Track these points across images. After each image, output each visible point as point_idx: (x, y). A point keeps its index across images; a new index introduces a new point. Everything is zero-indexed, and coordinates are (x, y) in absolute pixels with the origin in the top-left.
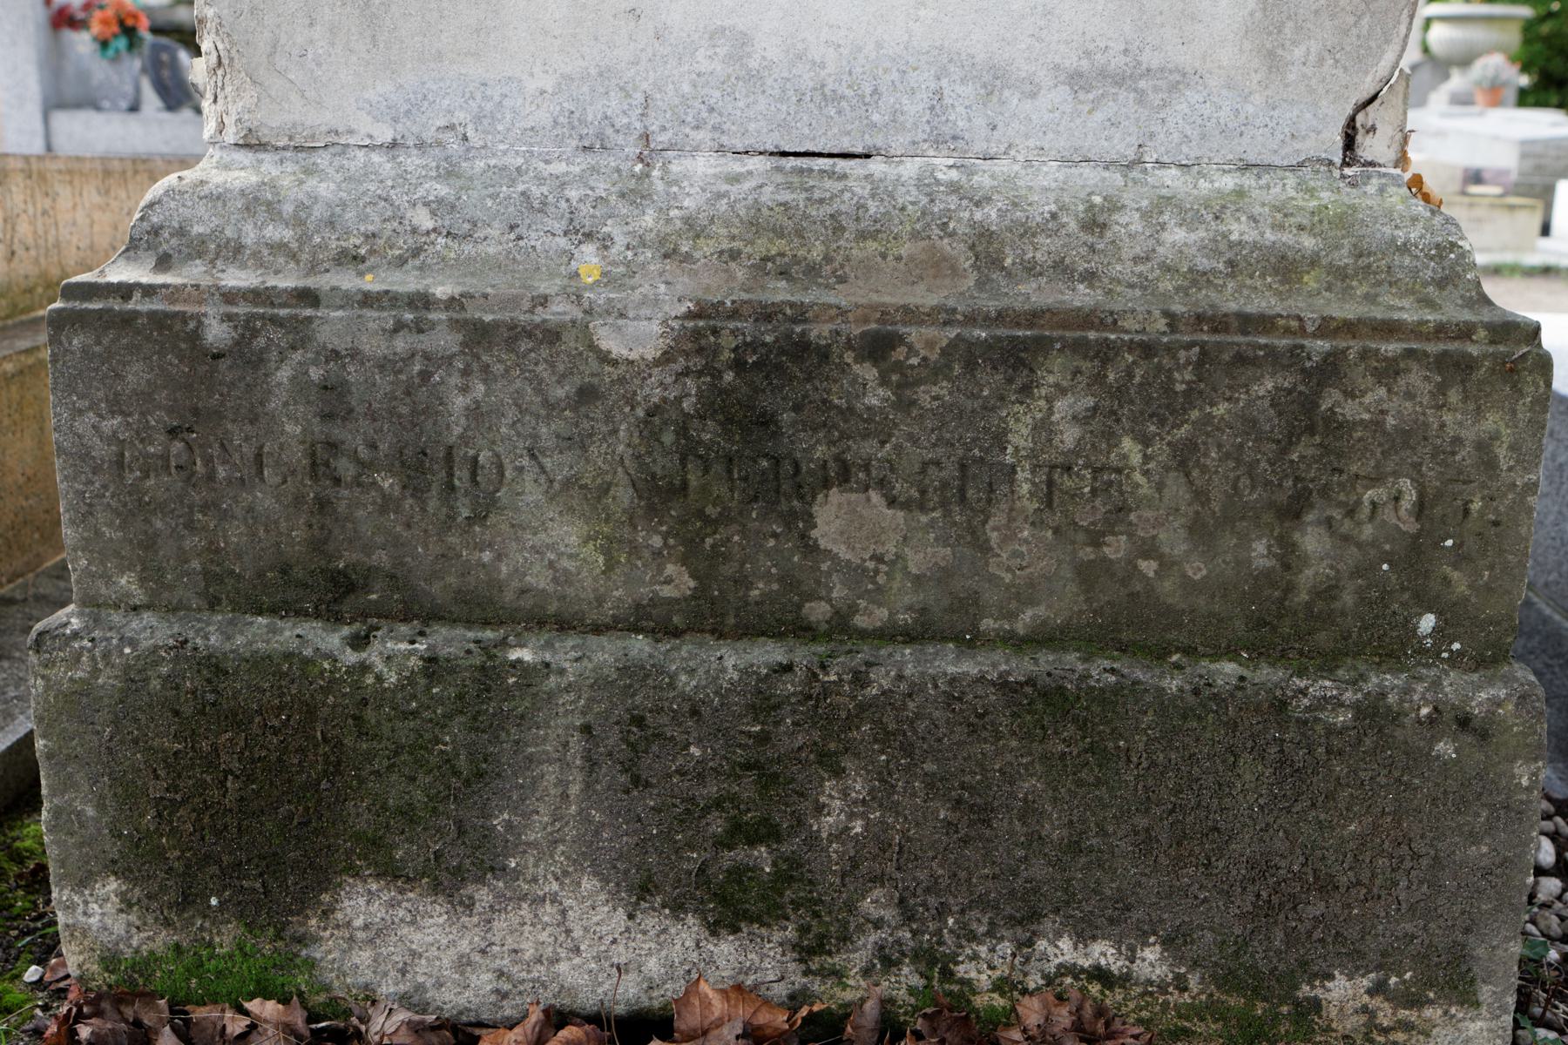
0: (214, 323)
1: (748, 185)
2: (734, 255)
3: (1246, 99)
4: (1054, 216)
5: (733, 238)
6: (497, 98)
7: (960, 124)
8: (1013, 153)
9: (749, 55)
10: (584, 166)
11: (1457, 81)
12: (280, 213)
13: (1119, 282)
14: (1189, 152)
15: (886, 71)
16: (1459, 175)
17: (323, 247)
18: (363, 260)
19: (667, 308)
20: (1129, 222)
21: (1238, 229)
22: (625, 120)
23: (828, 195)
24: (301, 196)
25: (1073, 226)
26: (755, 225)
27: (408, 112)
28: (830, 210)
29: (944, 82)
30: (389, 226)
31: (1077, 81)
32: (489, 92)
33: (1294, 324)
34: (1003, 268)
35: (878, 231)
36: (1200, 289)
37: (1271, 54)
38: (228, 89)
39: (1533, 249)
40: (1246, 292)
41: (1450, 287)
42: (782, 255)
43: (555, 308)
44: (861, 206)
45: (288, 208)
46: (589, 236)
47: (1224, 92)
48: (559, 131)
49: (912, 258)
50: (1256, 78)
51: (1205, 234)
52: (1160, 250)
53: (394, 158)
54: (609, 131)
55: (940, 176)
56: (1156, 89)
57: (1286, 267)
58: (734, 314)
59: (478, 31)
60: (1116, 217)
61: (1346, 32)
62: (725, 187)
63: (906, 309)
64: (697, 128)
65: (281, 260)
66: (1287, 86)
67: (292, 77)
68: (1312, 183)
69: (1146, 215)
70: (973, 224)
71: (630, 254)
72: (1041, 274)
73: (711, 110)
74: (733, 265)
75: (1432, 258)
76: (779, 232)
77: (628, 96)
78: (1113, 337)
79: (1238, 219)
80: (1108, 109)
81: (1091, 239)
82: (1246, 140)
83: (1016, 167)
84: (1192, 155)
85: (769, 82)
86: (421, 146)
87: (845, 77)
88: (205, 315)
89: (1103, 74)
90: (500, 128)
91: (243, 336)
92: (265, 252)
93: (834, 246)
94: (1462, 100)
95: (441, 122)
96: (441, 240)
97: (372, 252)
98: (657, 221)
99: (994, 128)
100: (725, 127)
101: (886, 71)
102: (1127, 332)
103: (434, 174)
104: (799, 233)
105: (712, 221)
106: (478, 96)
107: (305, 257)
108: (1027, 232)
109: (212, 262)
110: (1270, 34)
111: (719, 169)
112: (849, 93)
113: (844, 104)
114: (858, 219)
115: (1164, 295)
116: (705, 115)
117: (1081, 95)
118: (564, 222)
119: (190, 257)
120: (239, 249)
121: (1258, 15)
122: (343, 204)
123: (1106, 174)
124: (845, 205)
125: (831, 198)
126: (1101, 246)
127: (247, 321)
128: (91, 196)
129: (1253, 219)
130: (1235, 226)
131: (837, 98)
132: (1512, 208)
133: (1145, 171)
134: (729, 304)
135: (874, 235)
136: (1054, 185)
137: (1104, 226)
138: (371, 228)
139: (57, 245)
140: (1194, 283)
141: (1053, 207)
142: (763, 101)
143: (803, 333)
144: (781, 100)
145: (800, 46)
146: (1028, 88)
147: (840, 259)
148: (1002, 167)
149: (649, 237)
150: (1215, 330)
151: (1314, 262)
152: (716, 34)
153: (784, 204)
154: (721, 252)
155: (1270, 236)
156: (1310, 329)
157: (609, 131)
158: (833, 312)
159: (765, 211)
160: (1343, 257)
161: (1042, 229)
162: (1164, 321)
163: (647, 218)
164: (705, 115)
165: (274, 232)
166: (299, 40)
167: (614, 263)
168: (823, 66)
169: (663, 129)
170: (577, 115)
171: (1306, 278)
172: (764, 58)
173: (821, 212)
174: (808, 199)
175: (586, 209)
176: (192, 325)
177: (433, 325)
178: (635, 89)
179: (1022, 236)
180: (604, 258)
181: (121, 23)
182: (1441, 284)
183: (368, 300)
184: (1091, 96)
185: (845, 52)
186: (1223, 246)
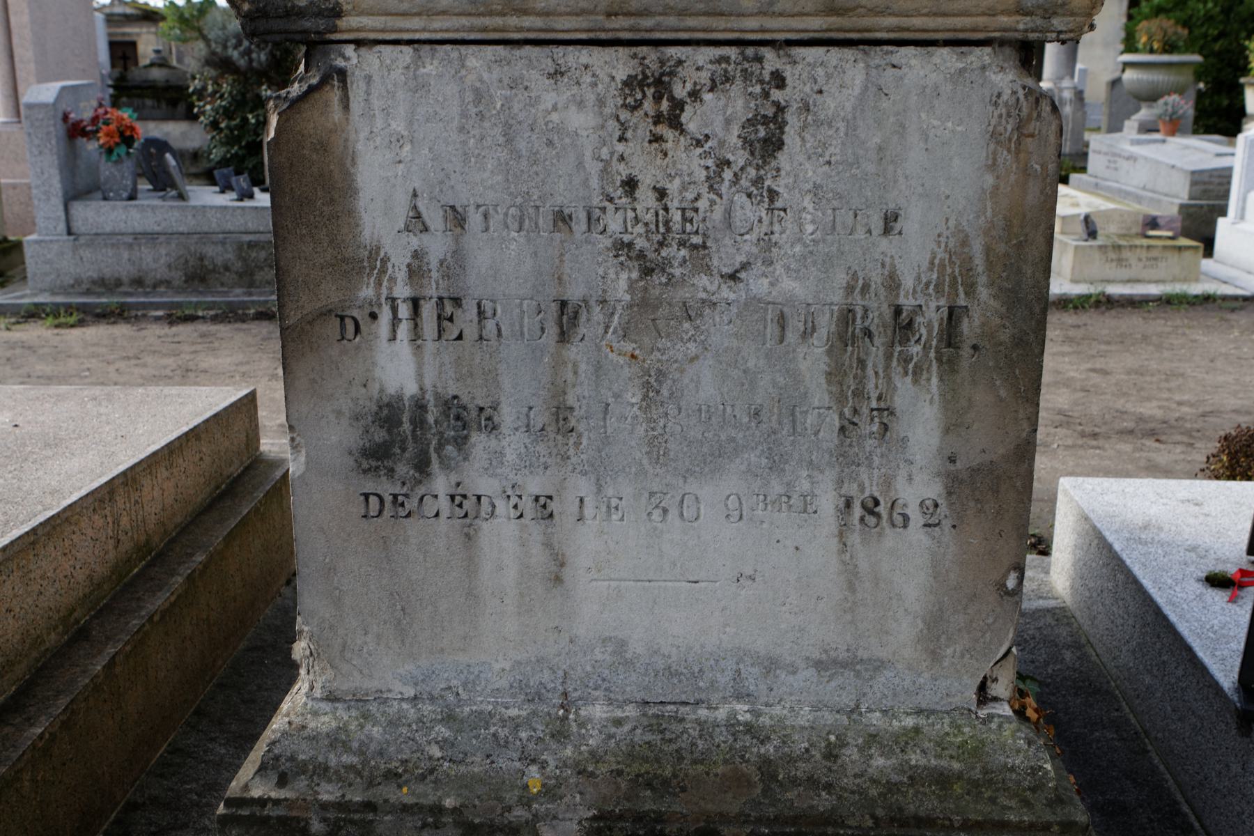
0: (316, 823)
1: (627, 728)
2: (620, 773)
3: (919, 675)
4: (807, 750)
5: (619, 763)
6: (476, 673)
7: (751, 688)
8: (783, 703)
9: (626, 651)
10: (529, 711)
11: (1144, 113)
12: (350, 748)
13: (846, 790)
14: (887, 703)
15: (707, 660)
16: (1141, 218)
17: (377, 767)
18: (400, 776)
19: (581, 813)
20: (851, 754)
21: (915, 758)
22: (553, 685)
23: (674, 736)
24: (363, 737)
25: (818, 756)
26: (631, 756)
27: (423, 681)
28: (674, 747)
29: (741, 666)
30: (415, 755)
31: (819, 665)
32: (472, 670)
33: (947, 823)
34: (778, 781)
35: (704, 759)
36: (893, 795)
37: (933, 652)
38: (317, 668)
39: (1196, 277)
40: (920, 796)
41: (1039, 792)
42: (648, 773)
43: (515, 813)
44: (694, 744)
45: (355, 745)
46: (533, 761)
47: (906, 671)
48: (513, 690)
49: (724, 775)
50: (925, 664)
51: (895, 761)
52: (870, 770)
53: (415, 705)
54: (543, 691)
55: (740, 718)
56: (866, 670)
57: (943, 780)
58: (621, 817)
59: (465, 638)
60: (843, 751)
61: (977, 641)
62: (613, 730)
63: (721, 814)
64: (595, 689)
65: (352, 776)
66: (943, 668)
67: (355, 663)
68: (959, 722)
69: (861, 749)
70: (759, 755)
71: (558, 771)
72: (800, 785)
73: (604, 680)
74: (619, 779)
75: (1029, 775)
76: (646, 760)
77: (554, 672)
78: (842, 832)
79: (915, 752)
80: (839, 681)
81: (829, 764)
82: (920, 696)
83: (785, 712)
84: (889, 704)
85: (638, 665)
86: (432, 699)
87: (683, 663)
88: (311, 818)
89: (835, 662)
90: (478, 689)
91: (332, 830)
92: (343, 771)
93: (678, 768)
94: (1147, 128)
95: (443, 686)
96: (446, 764)
97: (405, 771)
98: (573, 753)
99: (771, 690)
100: (612, 689)
101: (707, 660)
102: (850, 827)
103: (439, 717)
104: (658, 760)
105: (606, 753)
106: (465, 672)
107: (366, 773)
108: (791, 760)
109: (311, 777)
110: (932, 641)
111: (609, 714)
112: (685, 671)
113: (682, 677)
114: (692, 752)
115: (872, 799)
116: (600, 682)
117: (822, 673)
118: (519, 754)
119: (298, 774)
120: (327, 769)
121: (925, 631)
122: (388, 742)
123: (838, 716)
124: (684, 743)
125: (676, 739)
126: (835, 768)
127: (335, 822)
128: (163, 473)
129: (923, 751)
130: (913, 756)
131: (679, 674)
132: (1180, 248)
133: (860, 714)
134: (617, 811)
135: (702, 762)
136: (807, 724)
137: (836, 757)
138: (404, 757)
139: (144, 521)
140: (890, 791)
141: (806, 745)
142: (634, 677)
143: (661, 830)
144: (645, 675)
145: (656, 647)
146: (791, 669)
147: (682, 775)
148: (777, 710)
149: (569, 762)
150: (901, 826)
151: (960, 776)
152: (605, 641)
153: (648, 743)
154: (612, 771)
155: (933, 762)
156: (957, 825)
157: (543, 691)
158: (679, 816)
159: (637, 747)
160: (977, 774)
161: (800, 758)
162: (871, 821)
163: (567, 751)
164: (600, 682)
165: (347, 759)
166: (359, 642)
167: (549, 778)
168: (669, 657)
169: (575, 690)
170: (524, 682)
171: (955, 787)
172: (635, 653)
173: (670, 748)
174: (662, 739)
175: (531, 746)
176: (303, 824)
177: (445, 825)
178: (559, 668)
179: (788, 762)
180: (543, 774)
181: (121, 134)
182: (1033, 790)
183: (406, 808)
184: (828, 674)
185: (683, 649)
186: (906, 768)
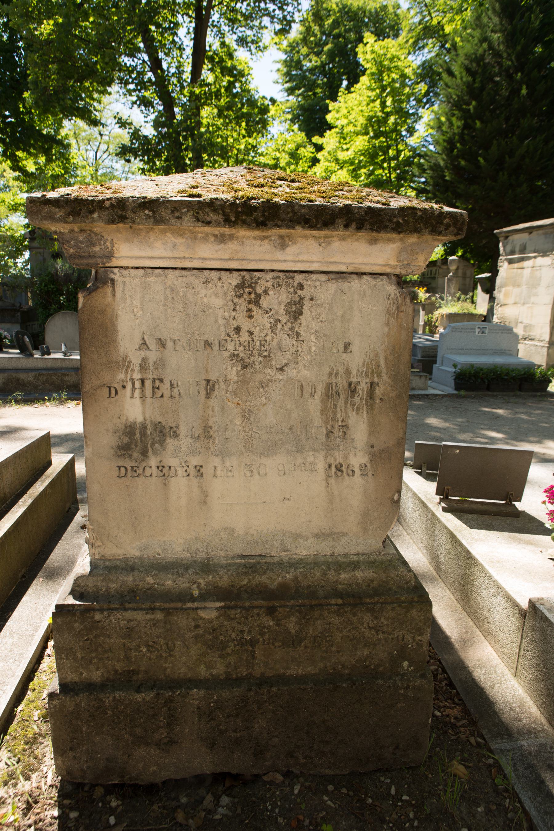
37: (365, 528)
89: (324, 534)
131: (258, 543)
152: (225, 529)
